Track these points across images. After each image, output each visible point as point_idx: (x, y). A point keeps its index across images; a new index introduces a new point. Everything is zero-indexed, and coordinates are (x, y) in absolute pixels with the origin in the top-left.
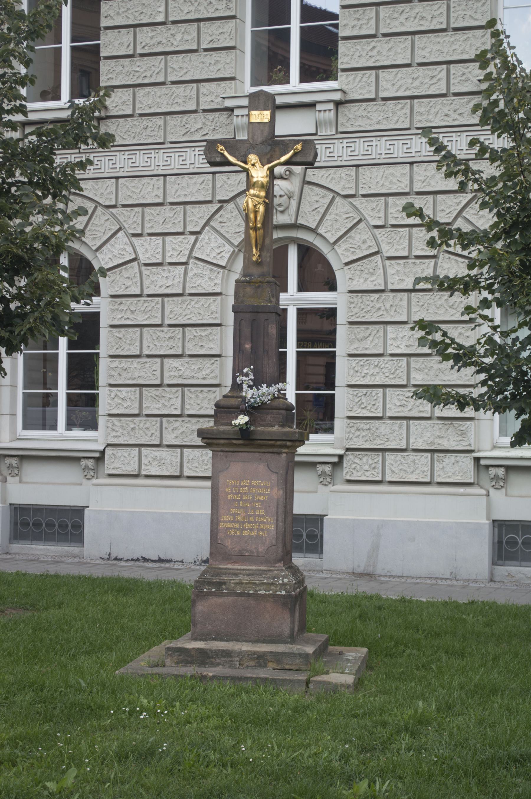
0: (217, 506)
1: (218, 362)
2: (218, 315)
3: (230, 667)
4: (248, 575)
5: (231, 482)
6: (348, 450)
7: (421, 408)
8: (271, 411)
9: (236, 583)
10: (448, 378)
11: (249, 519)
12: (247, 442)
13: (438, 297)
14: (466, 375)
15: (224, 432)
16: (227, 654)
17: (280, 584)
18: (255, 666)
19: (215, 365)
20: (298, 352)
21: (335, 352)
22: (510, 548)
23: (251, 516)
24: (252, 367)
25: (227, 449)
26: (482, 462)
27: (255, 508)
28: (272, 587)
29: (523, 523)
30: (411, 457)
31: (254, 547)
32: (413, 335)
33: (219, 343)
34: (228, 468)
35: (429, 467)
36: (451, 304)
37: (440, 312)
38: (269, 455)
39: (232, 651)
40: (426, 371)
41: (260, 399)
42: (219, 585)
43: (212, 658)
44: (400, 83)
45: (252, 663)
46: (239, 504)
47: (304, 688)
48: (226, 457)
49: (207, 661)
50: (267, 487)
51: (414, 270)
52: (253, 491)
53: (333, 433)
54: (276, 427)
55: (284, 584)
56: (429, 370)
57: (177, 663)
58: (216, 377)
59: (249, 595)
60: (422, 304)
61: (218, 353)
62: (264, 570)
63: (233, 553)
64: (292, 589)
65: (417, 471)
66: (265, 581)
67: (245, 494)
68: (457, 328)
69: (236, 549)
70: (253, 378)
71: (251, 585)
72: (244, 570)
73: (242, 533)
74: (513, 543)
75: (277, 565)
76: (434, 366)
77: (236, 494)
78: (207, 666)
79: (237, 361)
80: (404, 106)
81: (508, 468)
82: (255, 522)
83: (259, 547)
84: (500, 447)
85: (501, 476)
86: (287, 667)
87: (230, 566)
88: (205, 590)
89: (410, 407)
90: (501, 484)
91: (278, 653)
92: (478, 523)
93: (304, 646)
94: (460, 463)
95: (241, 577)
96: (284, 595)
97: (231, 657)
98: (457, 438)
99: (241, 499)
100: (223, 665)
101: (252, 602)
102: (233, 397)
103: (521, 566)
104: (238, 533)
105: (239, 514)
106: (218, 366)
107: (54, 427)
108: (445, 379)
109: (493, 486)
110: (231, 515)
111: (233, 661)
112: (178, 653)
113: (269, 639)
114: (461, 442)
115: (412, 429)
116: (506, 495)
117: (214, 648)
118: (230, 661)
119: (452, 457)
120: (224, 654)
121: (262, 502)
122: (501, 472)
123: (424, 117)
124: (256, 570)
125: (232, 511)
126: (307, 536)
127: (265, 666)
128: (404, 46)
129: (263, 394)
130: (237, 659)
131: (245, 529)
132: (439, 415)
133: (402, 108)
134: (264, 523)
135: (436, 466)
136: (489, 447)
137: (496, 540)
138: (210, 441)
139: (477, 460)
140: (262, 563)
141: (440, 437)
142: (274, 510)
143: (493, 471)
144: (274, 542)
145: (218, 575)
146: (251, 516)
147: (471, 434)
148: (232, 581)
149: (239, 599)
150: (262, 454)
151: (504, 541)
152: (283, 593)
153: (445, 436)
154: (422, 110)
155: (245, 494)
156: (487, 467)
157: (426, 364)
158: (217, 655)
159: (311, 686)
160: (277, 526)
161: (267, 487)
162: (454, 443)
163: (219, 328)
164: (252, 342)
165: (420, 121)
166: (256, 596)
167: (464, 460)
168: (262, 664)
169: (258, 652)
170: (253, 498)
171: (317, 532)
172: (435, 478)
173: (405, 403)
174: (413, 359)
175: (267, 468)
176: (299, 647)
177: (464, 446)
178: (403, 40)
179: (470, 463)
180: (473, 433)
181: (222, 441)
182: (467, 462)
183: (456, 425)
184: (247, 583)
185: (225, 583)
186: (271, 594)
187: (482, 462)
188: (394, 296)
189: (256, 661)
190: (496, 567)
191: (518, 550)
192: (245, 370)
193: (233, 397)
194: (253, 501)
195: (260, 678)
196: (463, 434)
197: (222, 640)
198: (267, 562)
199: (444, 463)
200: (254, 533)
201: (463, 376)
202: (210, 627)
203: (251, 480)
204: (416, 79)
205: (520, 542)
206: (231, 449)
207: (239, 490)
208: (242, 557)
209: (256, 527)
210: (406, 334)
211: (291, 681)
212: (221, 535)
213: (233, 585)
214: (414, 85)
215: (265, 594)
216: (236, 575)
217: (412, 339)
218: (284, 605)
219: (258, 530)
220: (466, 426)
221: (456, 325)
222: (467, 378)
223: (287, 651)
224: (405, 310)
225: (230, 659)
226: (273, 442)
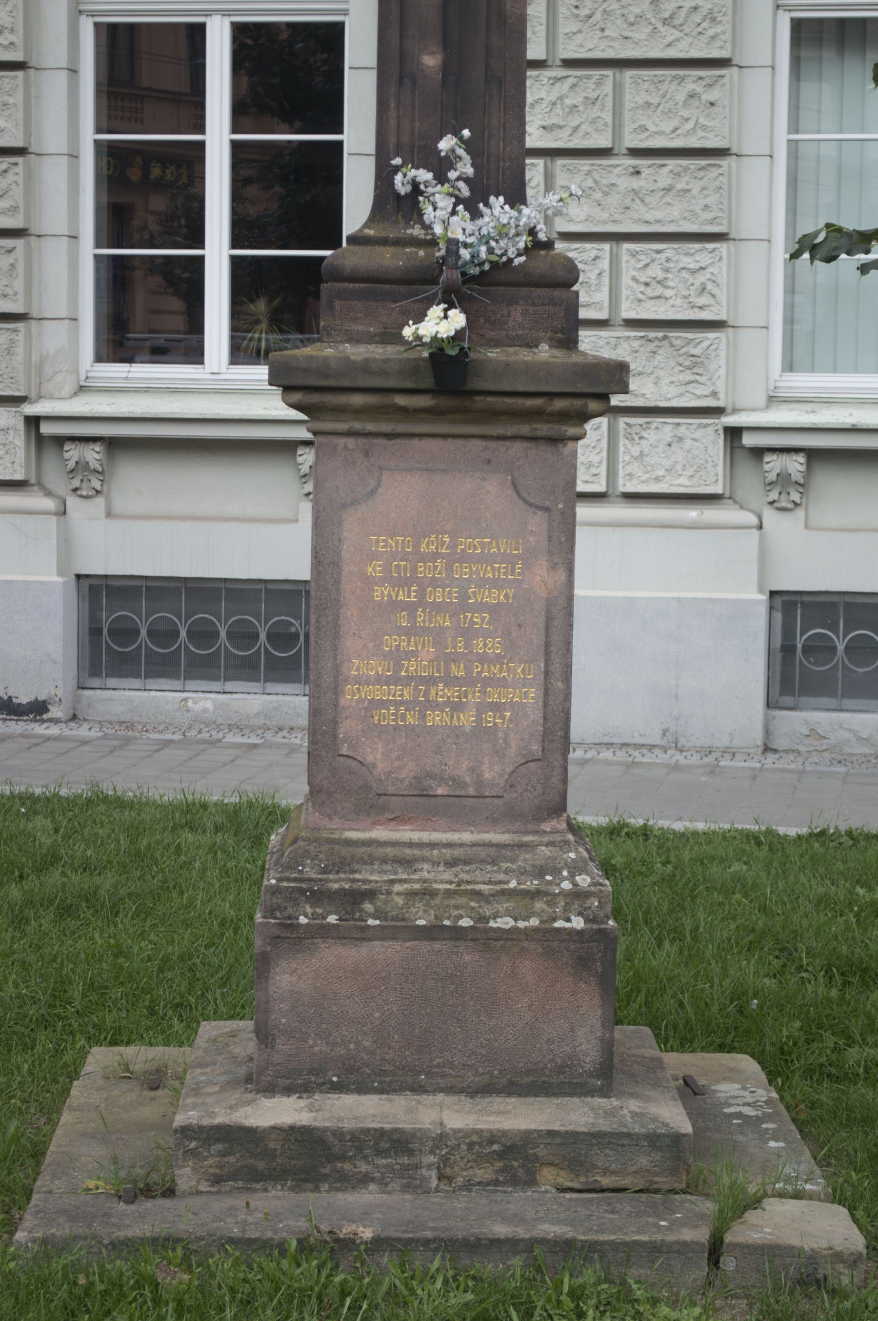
0: (336, 626)
1: (20, 169)
2: (17, 38)
3: (405, 1189)
4: (451, 864)
5: (383, 544)
8: (524, 291)
9: (411, 895)
10: (659, 215)
11: (448, 670)
12: (445, 402)
14: (706, 207)
15: (365, 367)
16: (397, 1143)
17: (564, 893)
18: (496, 1183)
19: (10, 177)
20: (235, 144)
21: (340, 144)
22: (816, 664)
23: (454, 659)
24: (466, 133)
25: (370, 427)
26: (748, 440)
27: (468, 633)
28: (539, 905)
29: (848, 599)
31: (466, 764)
32: (561, 98)
33: (20, 115)
34: (372, 493)
35: (604, 454)
36: (666, 15)
37: (636, 36)
38: (517, 447)
39: (413, 1134)
40: (598, 195)
41: (490, 251)
42: (352, 899)
43: (344, 1158)
45: (483, 1173)
46: (412, 617)
47: (702, 1271)
48: (366, 454)
49: (326, 1170)
50: (510, 560)
52: (462, 572)
53: (202, 362)
54: (544, 347)
55: (578, 895)
56: (606, 194)
57: (217, 1180)
58: (14, 209)
59: (457, 934)
60: (587, 12)
61: (20, 144)
62: (505, 846)
63: (391, 789)
64: (608, 909)
66: (513, 884)
67: (435, 583)
68: (683, 78)
69: (404, 773)
70: (470, 171)
71: (463, 900)
72: (432, 845)
74: (820, 649)
75: (546, 827)
76: (619, 182)
77: (403, 583)
78: (325, 1187)
79: (392, 114)
81: (813, 455)
82: (469, 681)
83: (485, 768)
84: (786, 401)
85: (797, 476)
86: (606, 1181)
87: (381, 833)
88: (303, 920)
90: (795, 496)
91: (574, 1134)
92: (737, 600)
93: (647, 1099)
94: (688, 444)
95: (426, 872)
96: (580, 933)
97: (411, 1153)
98: (681, 377)
99: (421, 602)
100: (383, 1183)
101: (468, 956)
102: (384, 242)
103: (842, 710)
104: (411, 720)
105: (414, 654)
106: (20, 179)
107: (194, 354)
108: (648, 217)
109: (772, 503)
110: (386, 656)
111: (417, 1167)
112: (220, 1146)
113: (527, 1080)
114: (689, 388)
116: (807, 526)
117: (348, 1125)
118: (407, 1168)
119: (665, 427)
120: (385, 1145)
121: (495, 610)
122: (796, 465)
124: (474, 845)
125: (390, 642)
126: (270, 637)
127: (531, 1182)
129: (502, 232)
130: (432, 1159)
131: (437, 706)
132: (632, 315)
134: (502, 683)
135: (622, 449)
136: (762, 401)
137: (778, 643)
138: (315, 398)
139: (733, 434)
140: (493, 821)
142: (537, 639)
143: (774, 464)
144: (536, 748)
145: (342, 865)
146: (454, 659)
147: (718, 365)
148: (397, 888)
149: (424, 946)
150: (493, 444)
151: (799, 646)
152: (578, 923)
153: (648, 370)
155: (435, 583)
156: (759, 453)
157: (597, 176)
158: (360, 1149)
159: (729, 1263)
160: (547, 692)
161: (510, 560)
162: (673, 391)
163: (20, 74)
164: (445, 46)
166: (483, 938)
167: (698, 434)
168: (520, 1173)
169: (504, 1133)
170: (464, 597)
171: (297, 626)
172: (621, 481)
174: (560, 162)
175: (510, 492)
176: (634, 1105)
177: (699, 397)
179: (714, 443)
180: (722, 361)
181: (357, 400)
182: (707, 439)
183: (678, 342)
184: (449, 893)
185: (371, 895)
186: (536, 930)
187: (748, 440)
189: (499, 1165)
190: (778, 713)
191: (836, 667)
192: (446, 144)
193: (384, 242)
194: (463, 606)
195: (541, 1241)
196: (695, 364)
197: (362, 1089)
198: (511, 815)
199: (643, 442)
200: (466, 720)
201: (698, 209)
202: (320, 1047)
203: (454, 537)
205: (841, 647)
206: (386, 427)
207: (415, 570)
208: (423, 800)
209: (474, 698)
210: (543, 95)
211: (655, 1249)
212: (348, 727)
213: (400, 901)
215: (514, 930)
216: (407, 863)
217: (558, 109)
218: (582, 964)
219: (481, 709)
220: (705, 344)
221: (681, 72)
222: (710, 216)
223: (604, 1125)
225: (406, 1160)
226: (538, 402)
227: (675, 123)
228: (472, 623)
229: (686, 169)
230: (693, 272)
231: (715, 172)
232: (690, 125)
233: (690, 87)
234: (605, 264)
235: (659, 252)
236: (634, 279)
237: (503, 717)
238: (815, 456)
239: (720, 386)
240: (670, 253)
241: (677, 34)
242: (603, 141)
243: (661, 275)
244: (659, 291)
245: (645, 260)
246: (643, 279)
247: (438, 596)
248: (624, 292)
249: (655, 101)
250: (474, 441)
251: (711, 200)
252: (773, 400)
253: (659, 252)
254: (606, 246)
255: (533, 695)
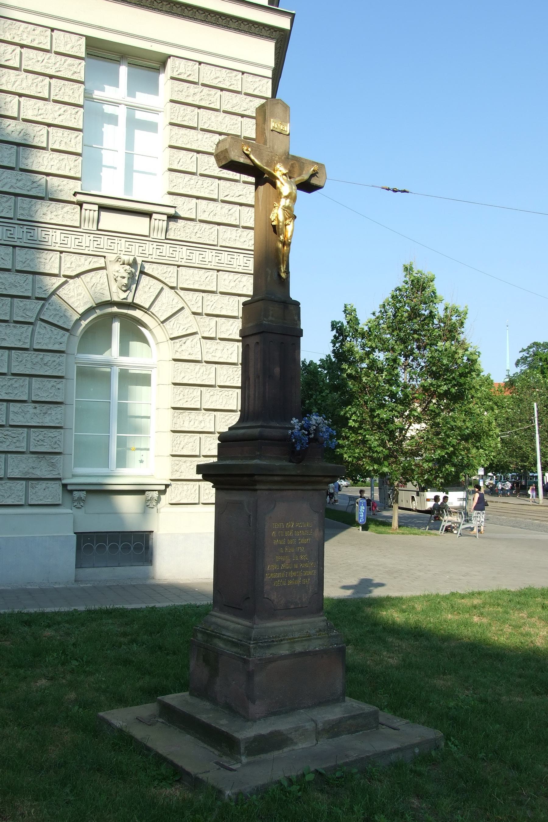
6: (171, 480)
7: (17, 444)
13: (35, 355)
26: (69, 488)
27: (298, 554)
30: (8, 484)
44: (5, 181)
51: (14, 333)
52: (297, 534)
56: (25, 414)
60: (21, 360)
65: (13, 496)
67: (290, 538)
68: (50, 381)
73: (287, 582)
80: (9, 200)
89: (8, 443)
90: (82, 504)
94: (50, 489)
98: (49, 469)
105: (285, 561)
114: (51, 472)
115: (10, 461)
119: (44, 484)
122: (83, 494)
123: (26, 212)
125: (278, 558)
128: (10, 152)
133: (7, 201)
136: (71, 476)
141: (33, 468)
153: (38, 467)
154: (25, 206)
155: (290, 538)
157: (23, 409)
165: (22, 214)
167: (54, 486)
170: (298, 541)
173: (4, 440)
178: (9, 147)
181: (276, 478)
182: (57, 487)
188: (174, 343)
204: (20, 180)
214: (17, 185)
220: (57, 459)
222: (58, 421)
224: (6, 364)
227: (47, 394)
228: (300, 550)
229: (51, 408)
230: (52, 438)
231: (60, 408)
232: (52, 395)
233: (52, 383)
234: (25, 435)
235: (42, 431)
236: (34, 439)
237: (308, 580)
238: (89, 492)
239: (61, 472)
240: (46, 432)
241: (49, 368)
242: (25, 398)
243: (43, 438)
244: (42, 443)
245: (38, 434)
246: (37, 439)
247: (290, 542)
248: (31, 444)
249: (41, 387)
250: (299, 491)
251: (59, 417)
252: (74, 476)
253: (42, 431)
254: (26, 429)
255: (315, 572)
